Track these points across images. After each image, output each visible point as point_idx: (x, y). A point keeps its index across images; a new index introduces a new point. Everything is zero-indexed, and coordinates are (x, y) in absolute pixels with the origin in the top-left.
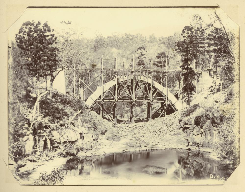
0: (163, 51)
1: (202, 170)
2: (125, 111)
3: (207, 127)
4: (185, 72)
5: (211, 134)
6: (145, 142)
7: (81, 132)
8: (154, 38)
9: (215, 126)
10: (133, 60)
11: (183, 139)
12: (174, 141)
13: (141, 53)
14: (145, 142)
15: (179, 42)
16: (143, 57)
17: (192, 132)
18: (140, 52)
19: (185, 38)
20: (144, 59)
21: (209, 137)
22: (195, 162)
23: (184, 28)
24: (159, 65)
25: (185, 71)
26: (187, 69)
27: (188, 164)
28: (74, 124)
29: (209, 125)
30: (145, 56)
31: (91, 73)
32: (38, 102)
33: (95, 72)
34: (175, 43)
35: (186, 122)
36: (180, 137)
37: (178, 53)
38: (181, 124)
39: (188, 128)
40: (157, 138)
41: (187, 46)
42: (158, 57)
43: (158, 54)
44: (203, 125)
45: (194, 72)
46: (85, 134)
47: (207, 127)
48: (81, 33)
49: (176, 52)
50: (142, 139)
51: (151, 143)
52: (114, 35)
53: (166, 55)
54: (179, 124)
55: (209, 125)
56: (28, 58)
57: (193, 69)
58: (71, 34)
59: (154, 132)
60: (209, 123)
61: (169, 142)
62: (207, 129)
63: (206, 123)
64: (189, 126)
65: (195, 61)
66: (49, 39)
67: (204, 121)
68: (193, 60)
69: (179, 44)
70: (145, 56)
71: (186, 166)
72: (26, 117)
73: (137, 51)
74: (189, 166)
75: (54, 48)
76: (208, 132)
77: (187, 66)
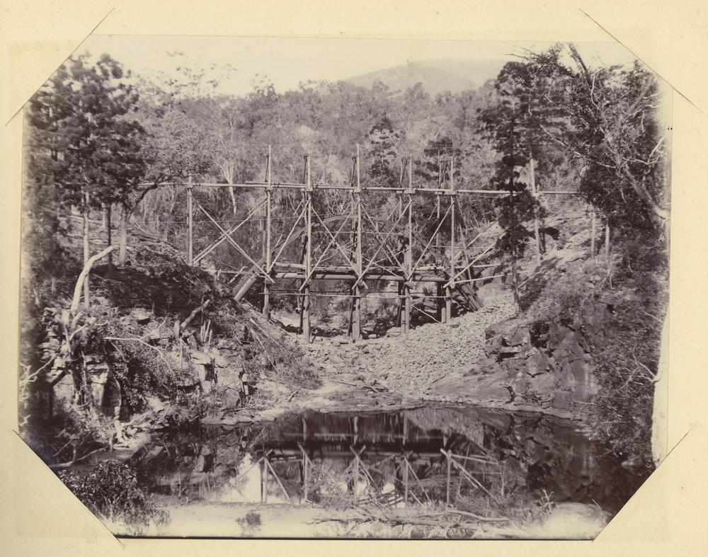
0: (444, 134)
1: (550, 464)
2: (335, 306)
3: (565, 354)
4: (507, 195)
5: (578, 374)
6: (390, 391)
7: (207, 361)
8: (422, 97)
9: (588, 350)
10: (358, 159)
11: (497, 385)
12: (472, 390)
13: (382, 141)
14: (390, 391)
15: (490, 110)
16: (386, 151)
17: (524, 367)
18: (381, 138)
19: (506, 98)
20: (389, 158)
21: (570, 382)
22: (531, 441)
23: (505, 67)
24: (435, 174)
25: (505, 193)
26: (510, 187)
27: (511, 448)
28: (188, 340)
29: (571, 347)
30: (393, 149)
31: (239, 197)
32: (86, 275)
33: (249, 194)
34: (479, 110)
35: (506, 338)
36: (490, 379)
37: (485, 140)
38: (492, 344)
39: (511, 355)
40: (424, 381)
41: (513, 120)
42: (429, 152)
43: (431, 142)
44: (556, 347)
45: (529, 196)
46: (219, 366)
47: (565, 354)
48: (215, 65)
49: (479, 137)
50: (384, 383)
51: (406, 394)
52: (306, 88)
53: (455, 146)
54: (486, 343)
55: (571, 347)
56: (57, 151)
57: (528, 188)
58: (181, 85)
59: (416, 365)
60: (569, 342)
61: (457, 394)
62: (564, 357)
63: (564, 342)
64: (516, 350)
65: (533, 163)
66: (116, 99)
67: (557, 335)
68: (528, 162)
69: (489, 118)
70: (393, 149)
71: (506, 451)
72: (133, 108)
73: (372, 133)
74: (513, 453)
75: (129, 125)
76: (568, 367)
77: (512, 180)
